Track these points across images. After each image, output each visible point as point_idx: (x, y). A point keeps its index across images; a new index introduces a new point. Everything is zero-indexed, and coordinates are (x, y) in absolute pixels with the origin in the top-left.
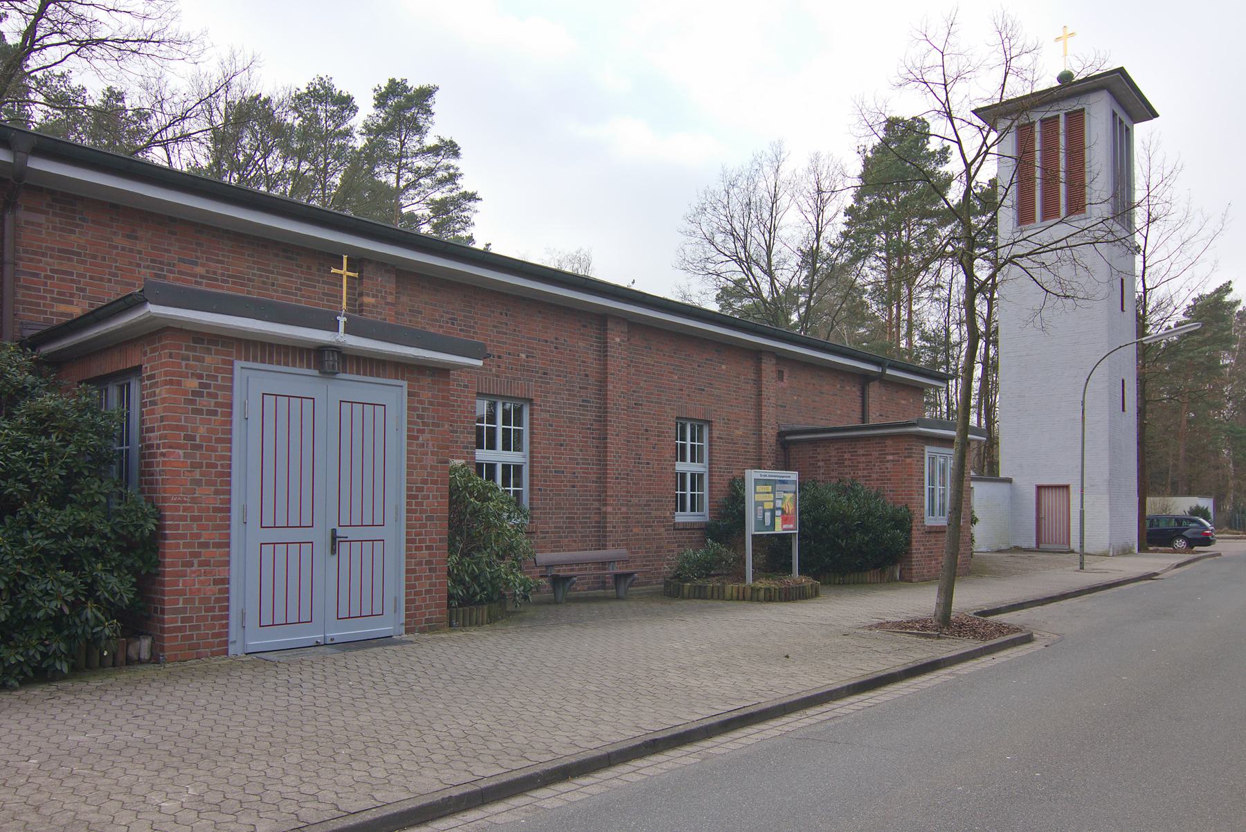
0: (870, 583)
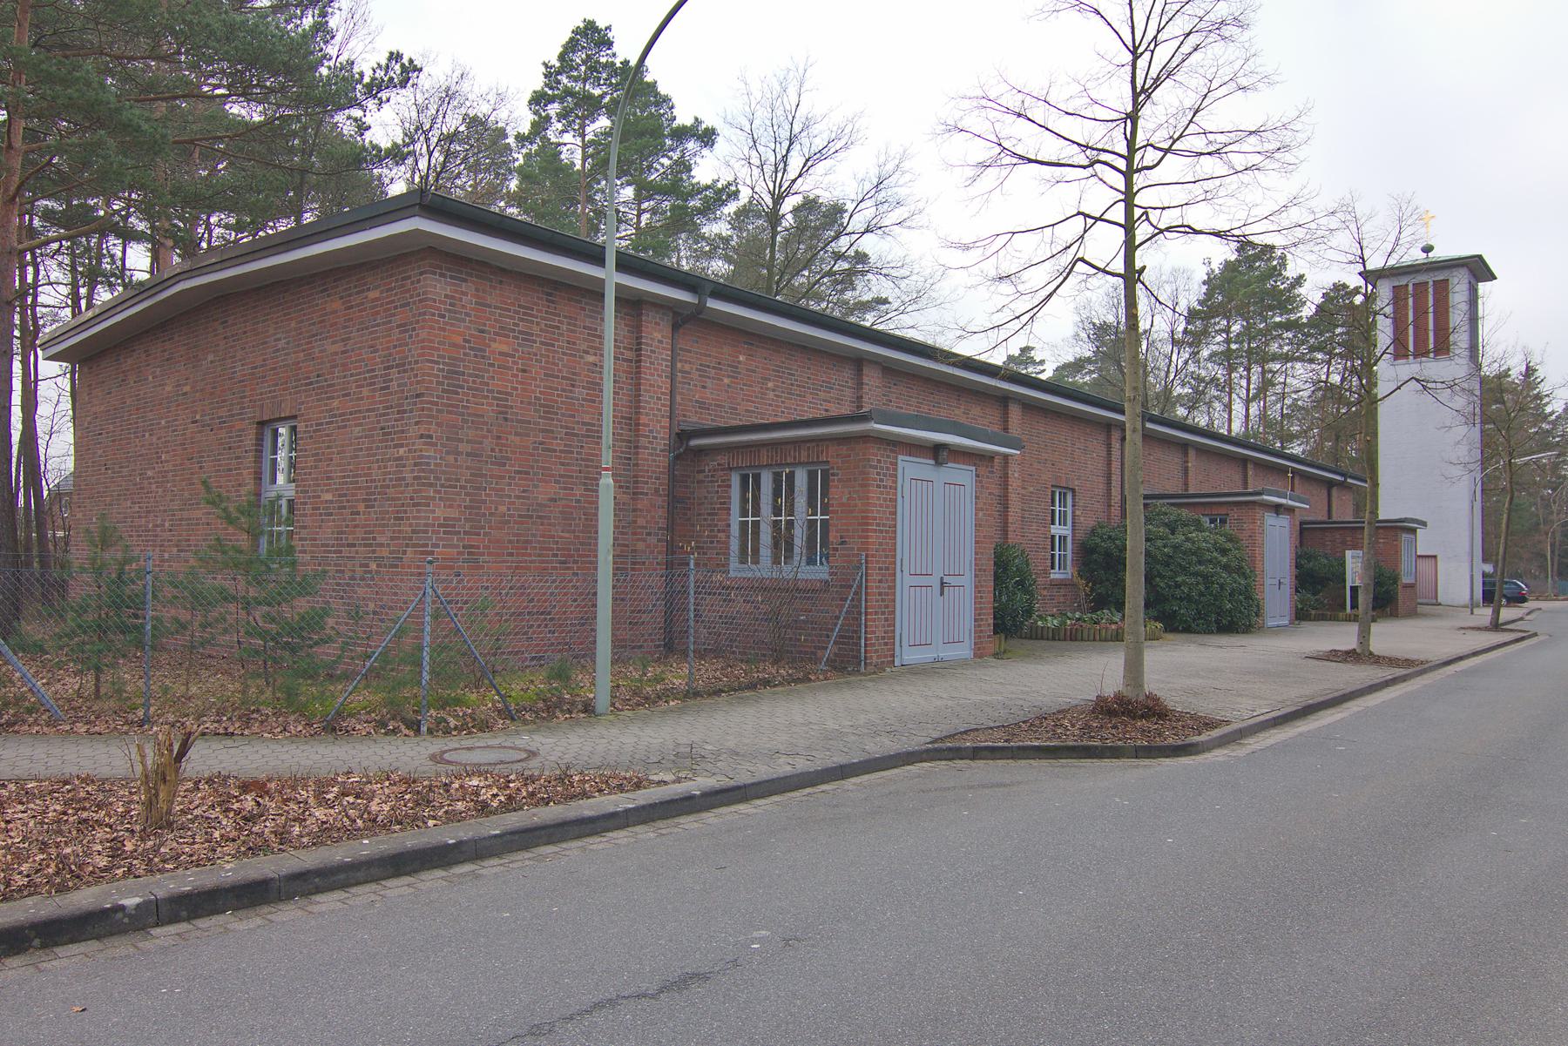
0: (1094, 640)
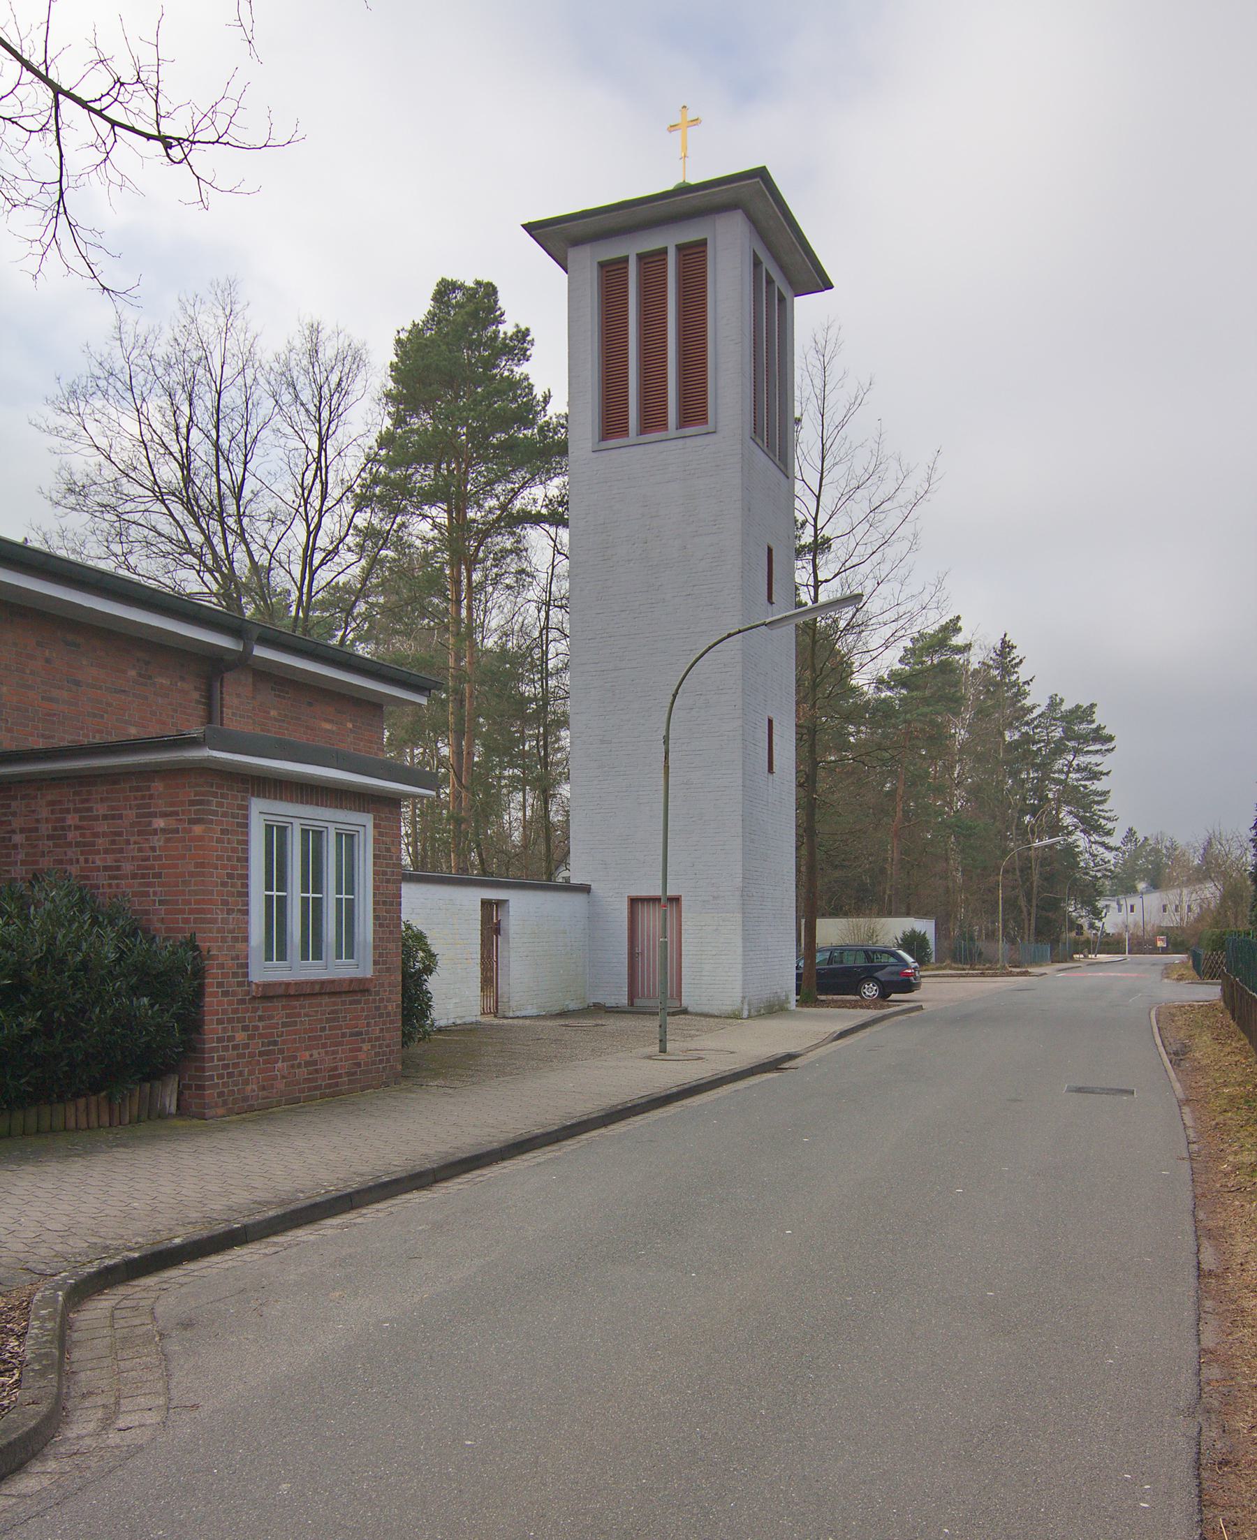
0: (77, 1129)
